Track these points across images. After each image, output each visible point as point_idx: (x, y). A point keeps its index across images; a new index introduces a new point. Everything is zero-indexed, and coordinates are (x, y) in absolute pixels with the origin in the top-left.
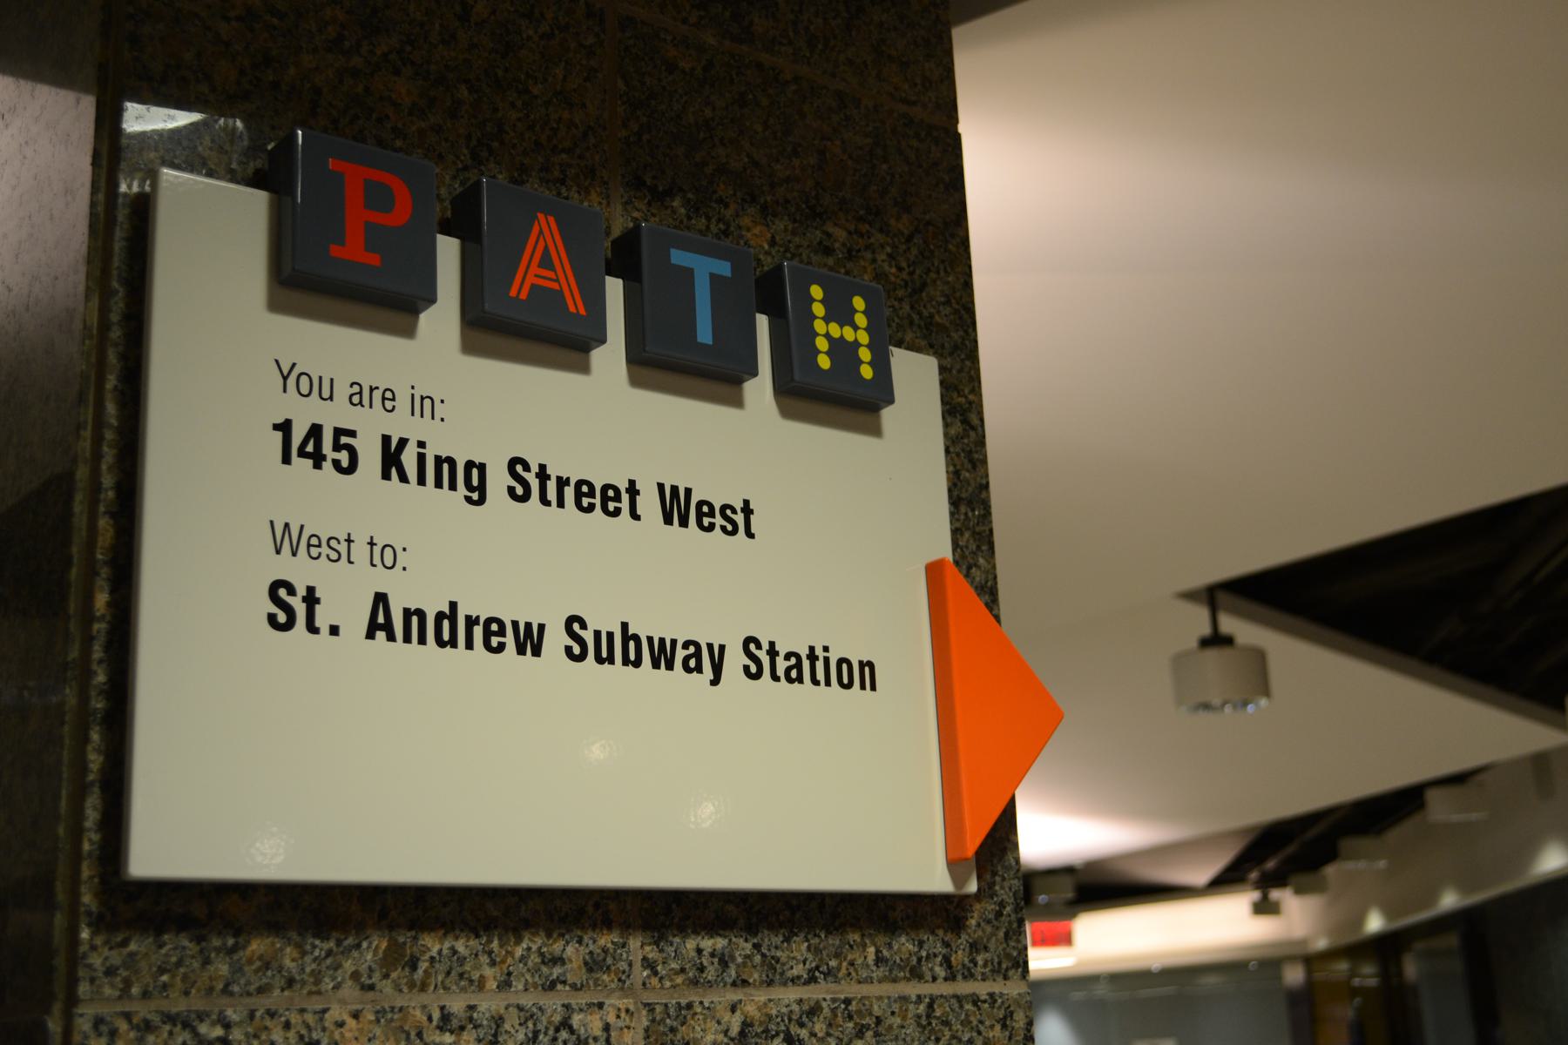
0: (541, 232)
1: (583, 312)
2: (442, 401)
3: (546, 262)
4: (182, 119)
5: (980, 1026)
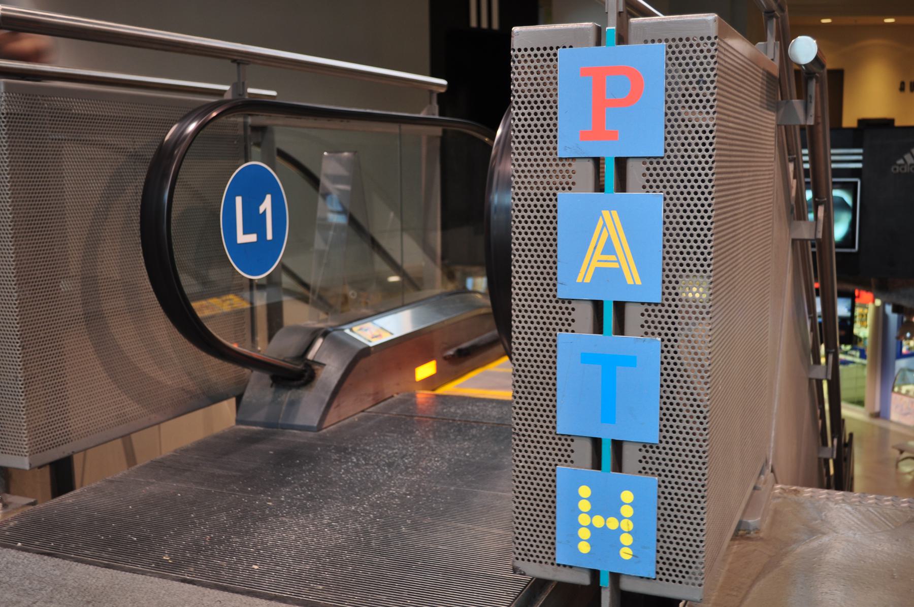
0: (604, 225)
1: (638, 282)
3: (609, 249)
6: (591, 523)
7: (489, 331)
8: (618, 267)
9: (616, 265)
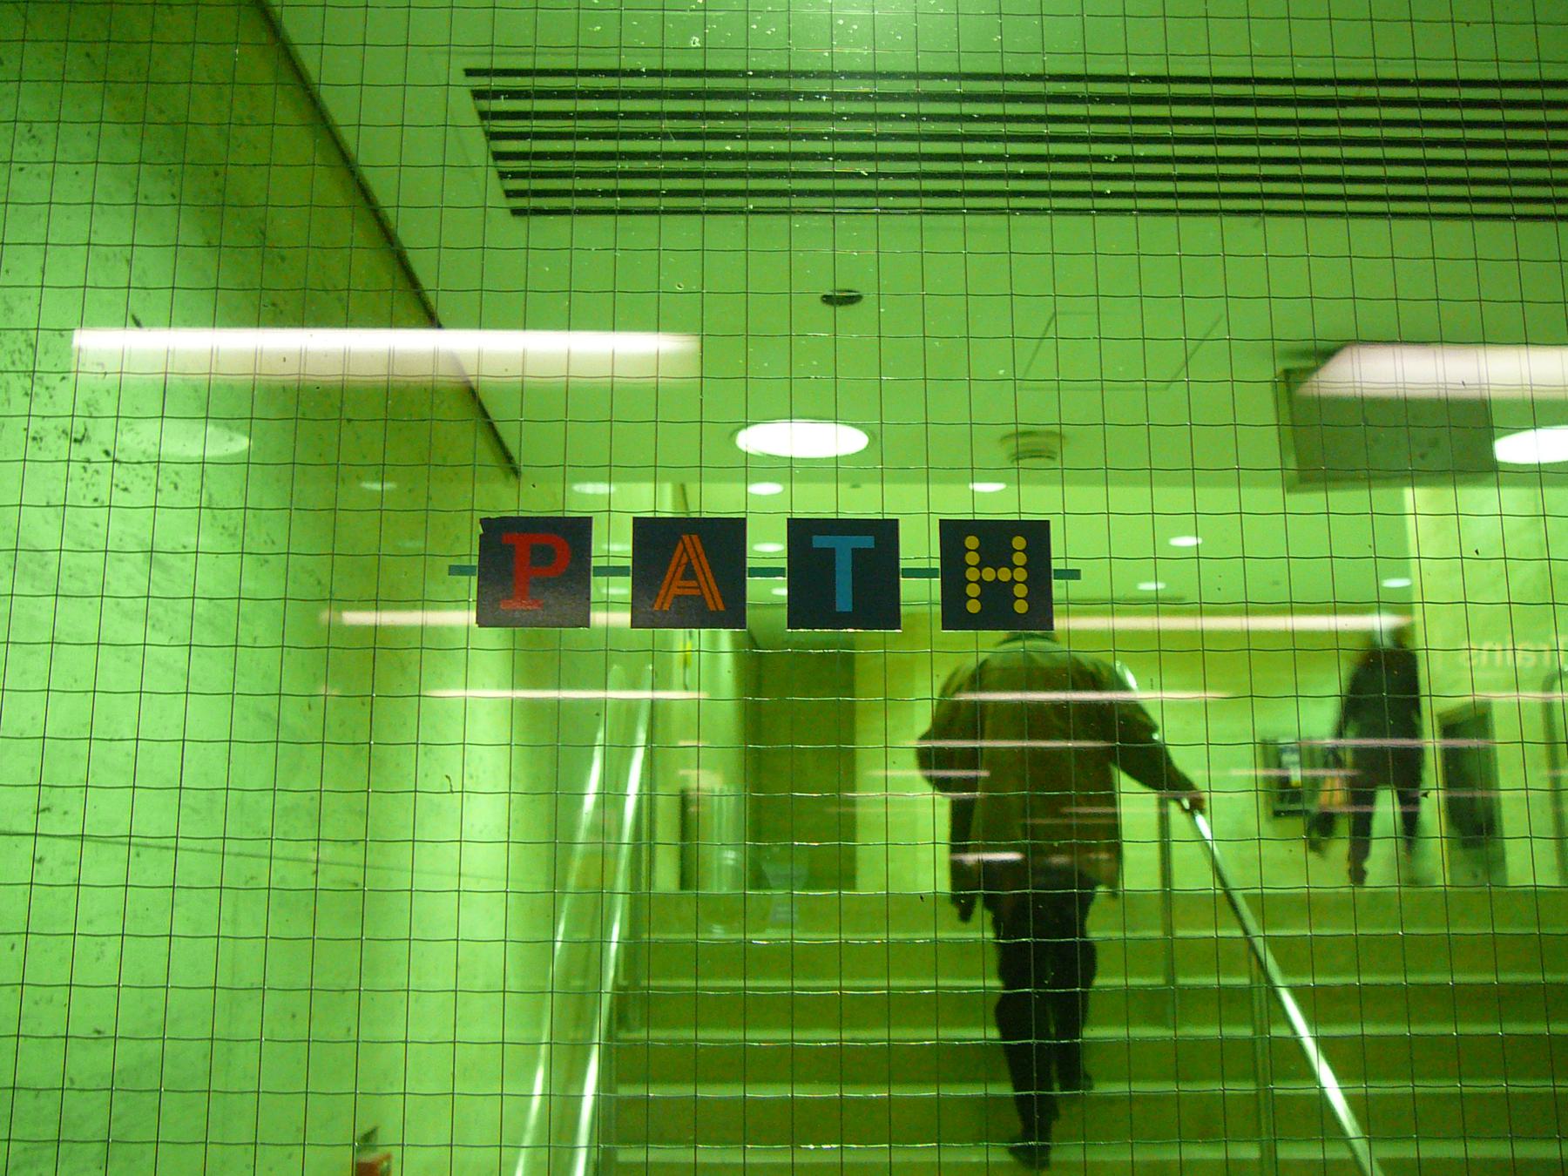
0: (685, 549)
1: (721, 608)
2: (7, 271)
3: (689, 574)
4: (1000, 486)
5: (17, 353)
6: (1012, 572)
7: (669, 15)
8: (700, 594)
9: (696, 592)
